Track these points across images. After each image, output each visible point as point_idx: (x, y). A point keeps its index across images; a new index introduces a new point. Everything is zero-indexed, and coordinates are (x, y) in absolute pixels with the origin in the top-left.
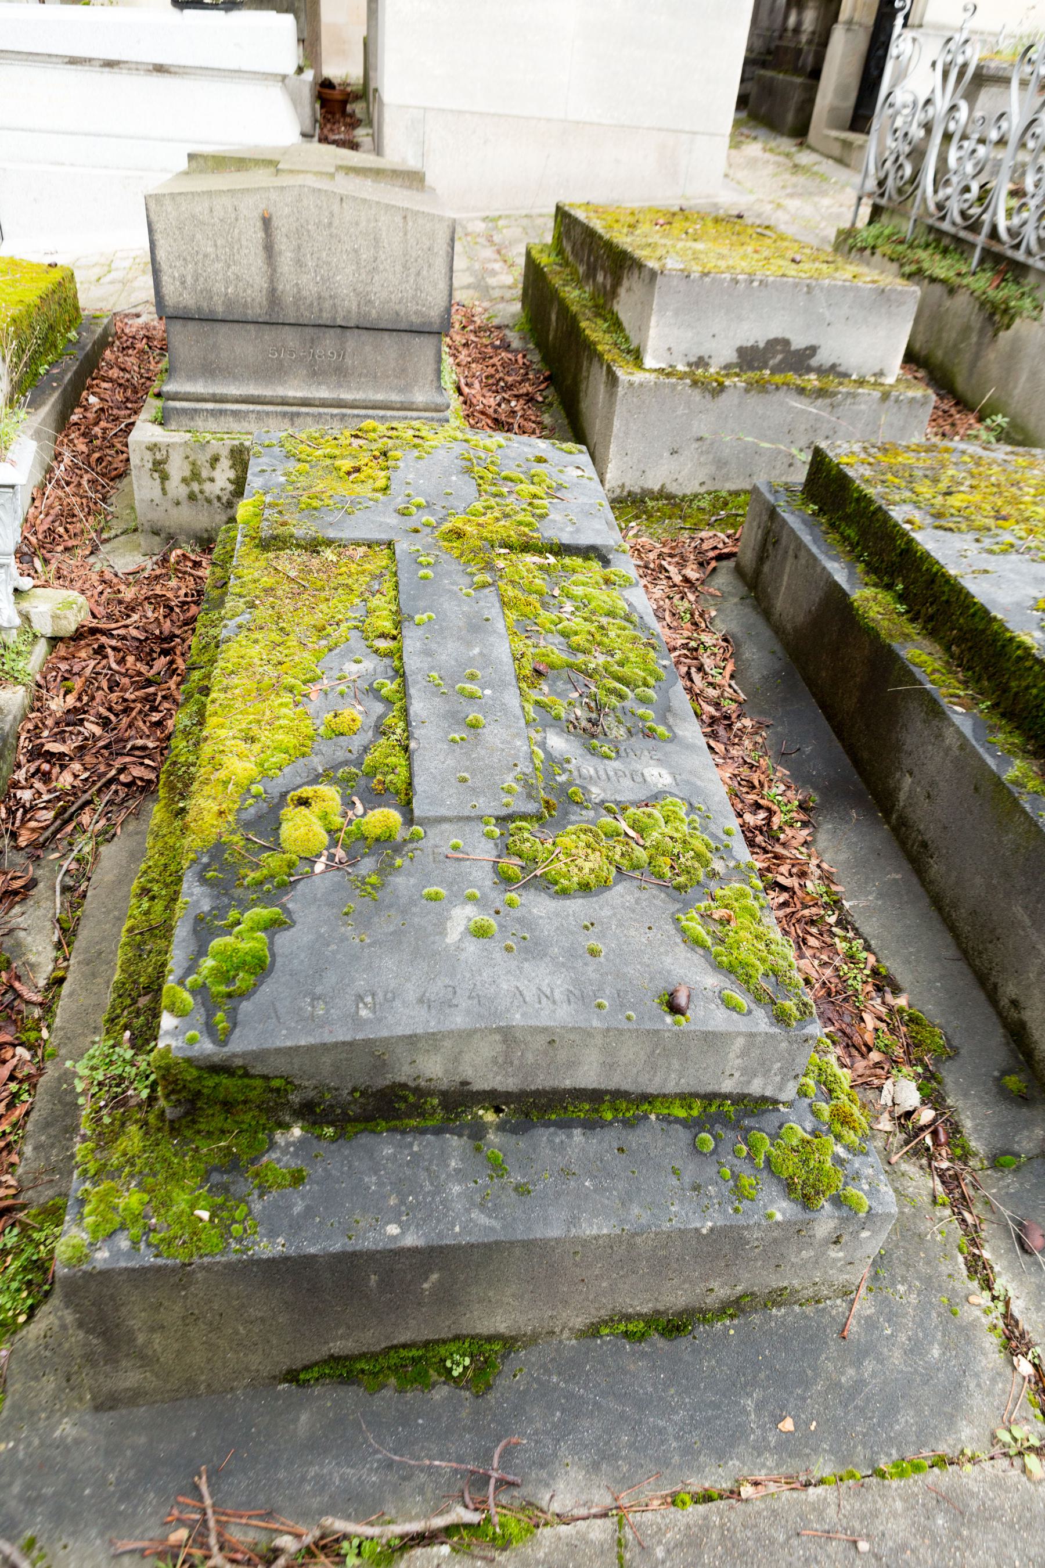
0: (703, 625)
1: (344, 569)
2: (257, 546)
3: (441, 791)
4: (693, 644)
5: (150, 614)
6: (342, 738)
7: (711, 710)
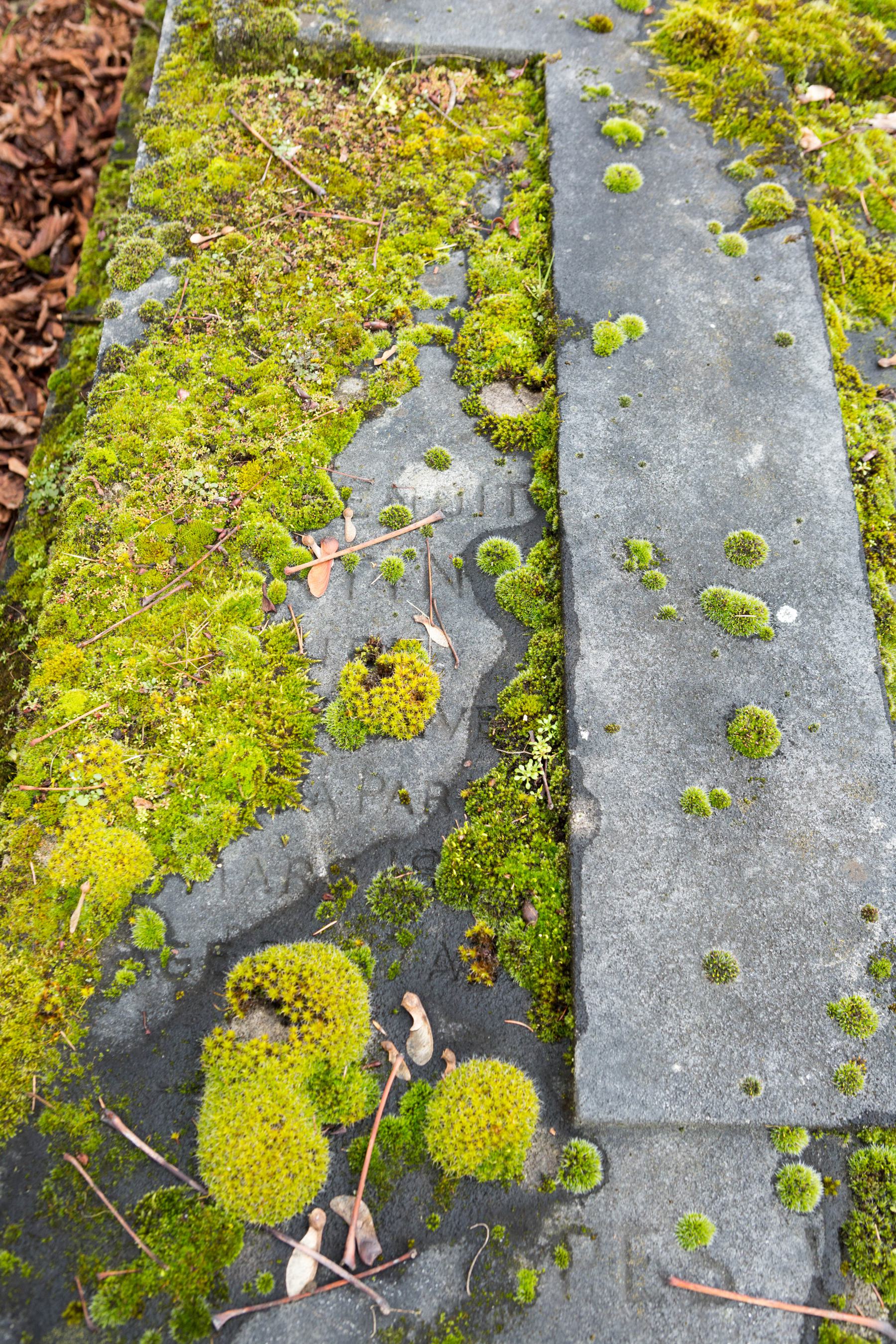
1: (414, 141)
2: (204, 56)
3: (659, 1014)
5: (39, 103)
6: (385, 746)
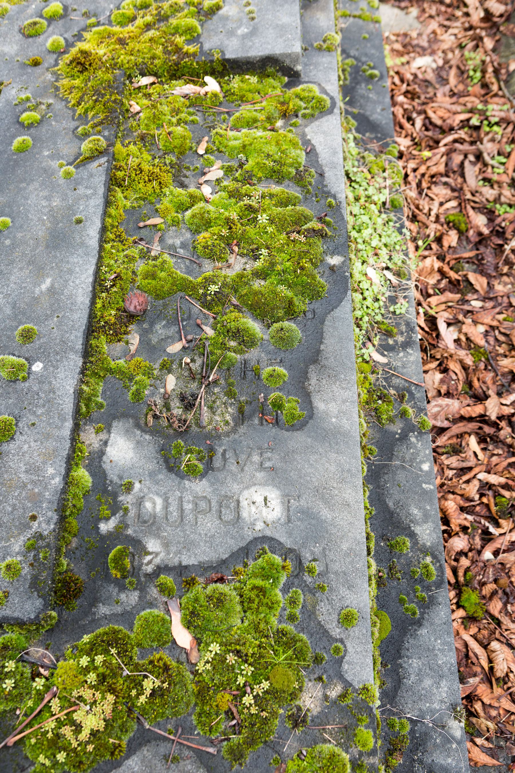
0: (495, 88)
4: (475, 121)
7: (480, 221)
